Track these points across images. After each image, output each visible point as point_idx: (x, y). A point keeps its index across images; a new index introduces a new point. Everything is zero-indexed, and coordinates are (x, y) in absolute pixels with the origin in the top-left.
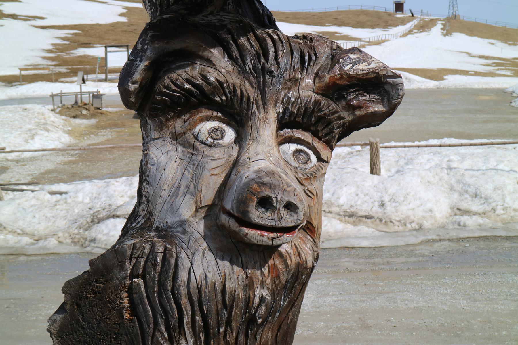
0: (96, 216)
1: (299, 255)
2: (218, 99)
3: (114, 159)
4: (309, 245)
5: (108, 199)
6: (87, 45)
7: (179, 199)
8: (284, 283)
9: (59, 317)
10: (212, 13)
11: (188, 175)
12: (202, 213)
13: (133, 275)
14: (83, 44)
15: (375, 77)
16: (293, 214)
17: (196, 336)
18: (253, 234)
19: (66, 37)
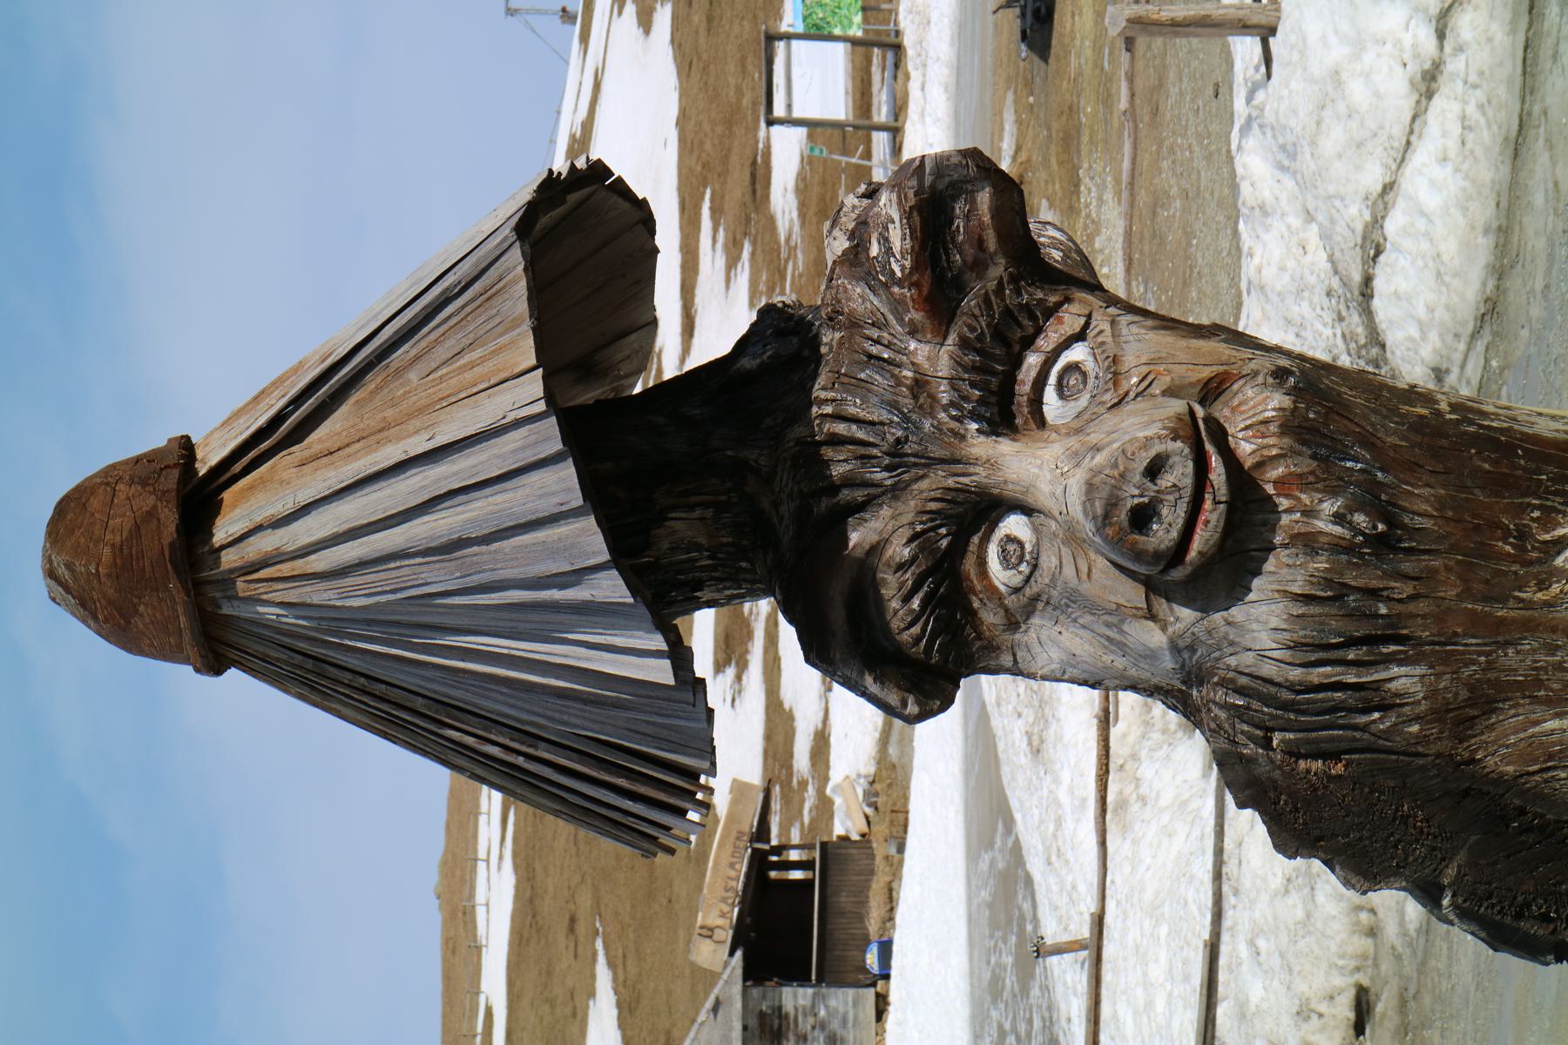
0: (1360, 348)
1: (1266, 422)
2: (944, 543)
3: (1185, 194)
4: (1250, 393)
5: (1306, 294)
6: (759, 176)
7: (1130, 641)
8: (1315, 464)
9: (1338, 868)
10: (776, 505)
11: (1087, 619)
12: (1161, 605)
13: (1266, 743)
14: (754, 192)
15: (920, 212)
16: (1171, 461)
17: (1388, 660)
18: (1200, 542)
19: (726, 248)
